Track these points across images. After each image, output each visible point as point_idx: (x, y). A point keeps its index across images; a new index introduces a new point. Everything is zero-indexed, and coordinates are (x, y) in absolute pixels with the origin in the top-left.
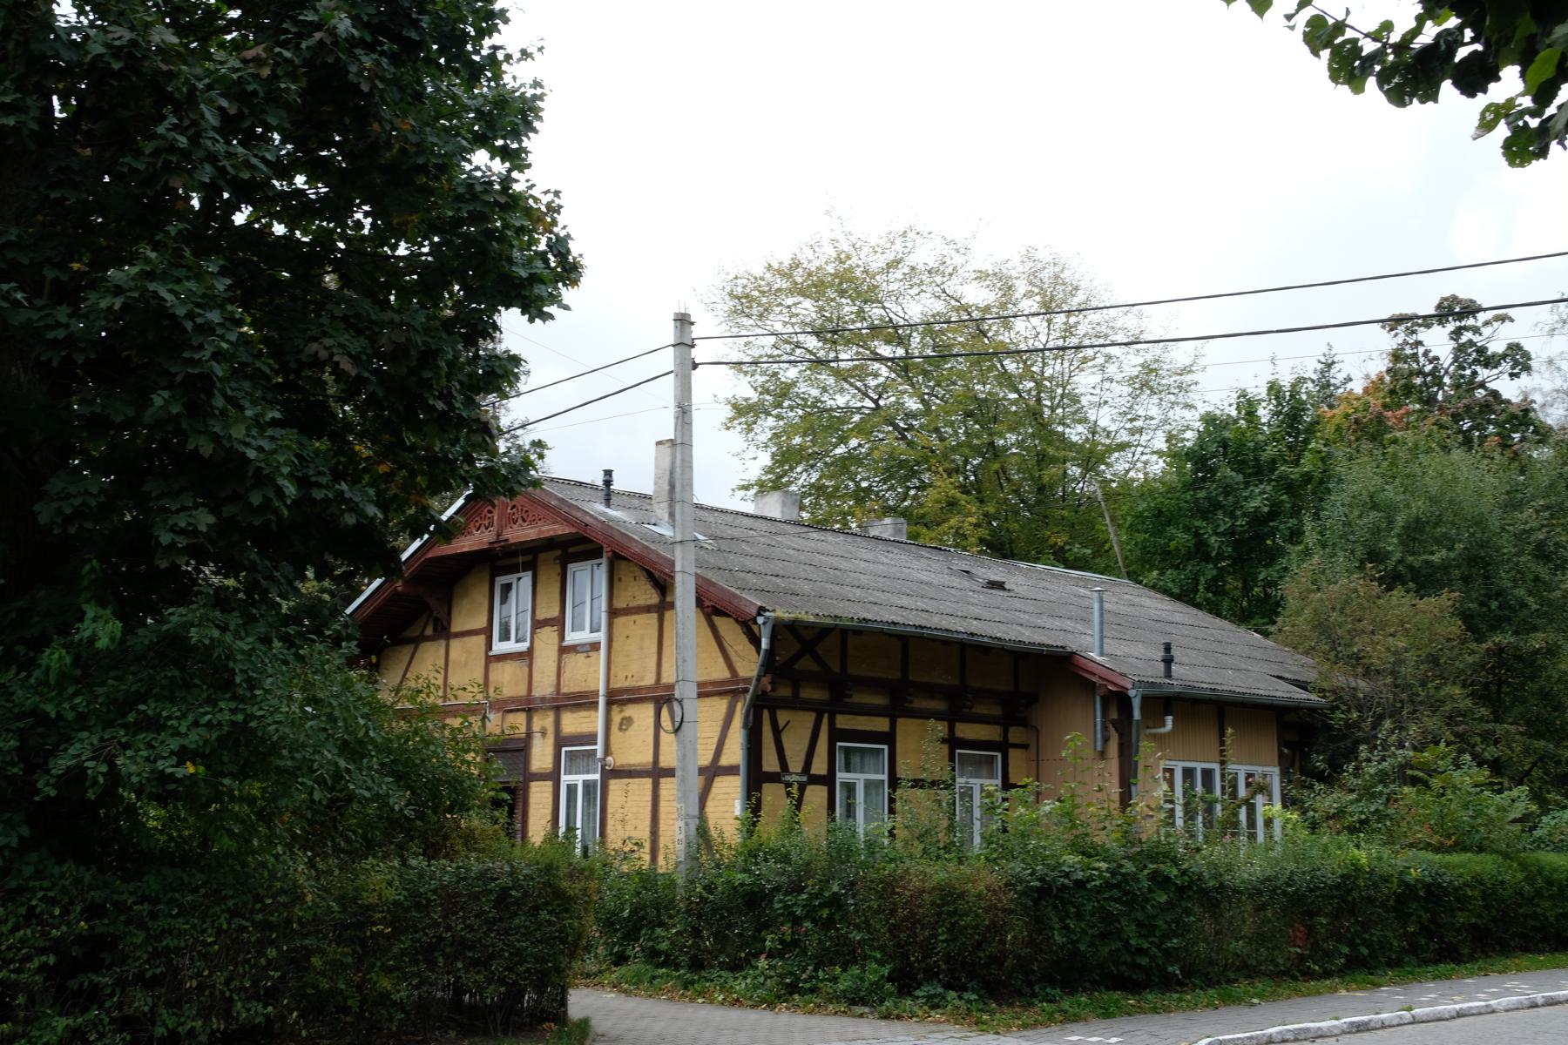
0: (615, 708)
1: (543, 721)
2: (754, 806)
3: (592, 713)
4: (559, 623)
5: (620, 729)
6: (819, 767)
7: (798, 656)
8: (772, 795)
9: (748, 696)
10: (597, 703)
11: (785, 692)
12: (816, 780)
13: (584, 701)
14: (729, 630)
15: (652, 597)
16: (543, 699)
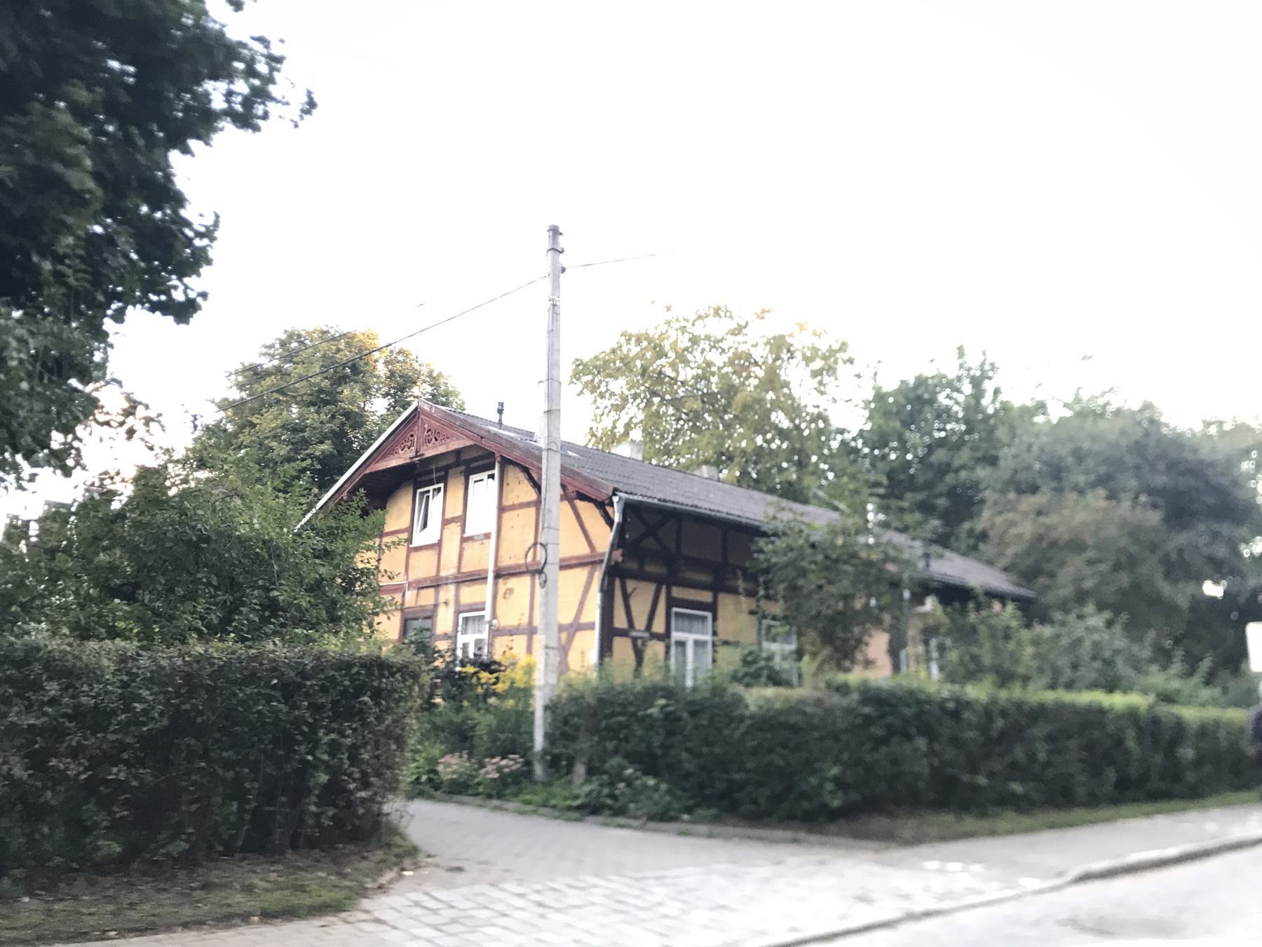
0: (501, 581)
1: (448, 593)
2: (606, 648)
3: (484, 586)
4: (462, 520)
5: (504, 598)
6: (659, 627)
7: (644, 536)
8: (622, 647)
9: (604, 565)
10: (486, 578)
11: (633, 565)
12: (655, 636)
13: (477, 578)
14: (589, 512)
15: (531, 495)
16: (447, 578)
